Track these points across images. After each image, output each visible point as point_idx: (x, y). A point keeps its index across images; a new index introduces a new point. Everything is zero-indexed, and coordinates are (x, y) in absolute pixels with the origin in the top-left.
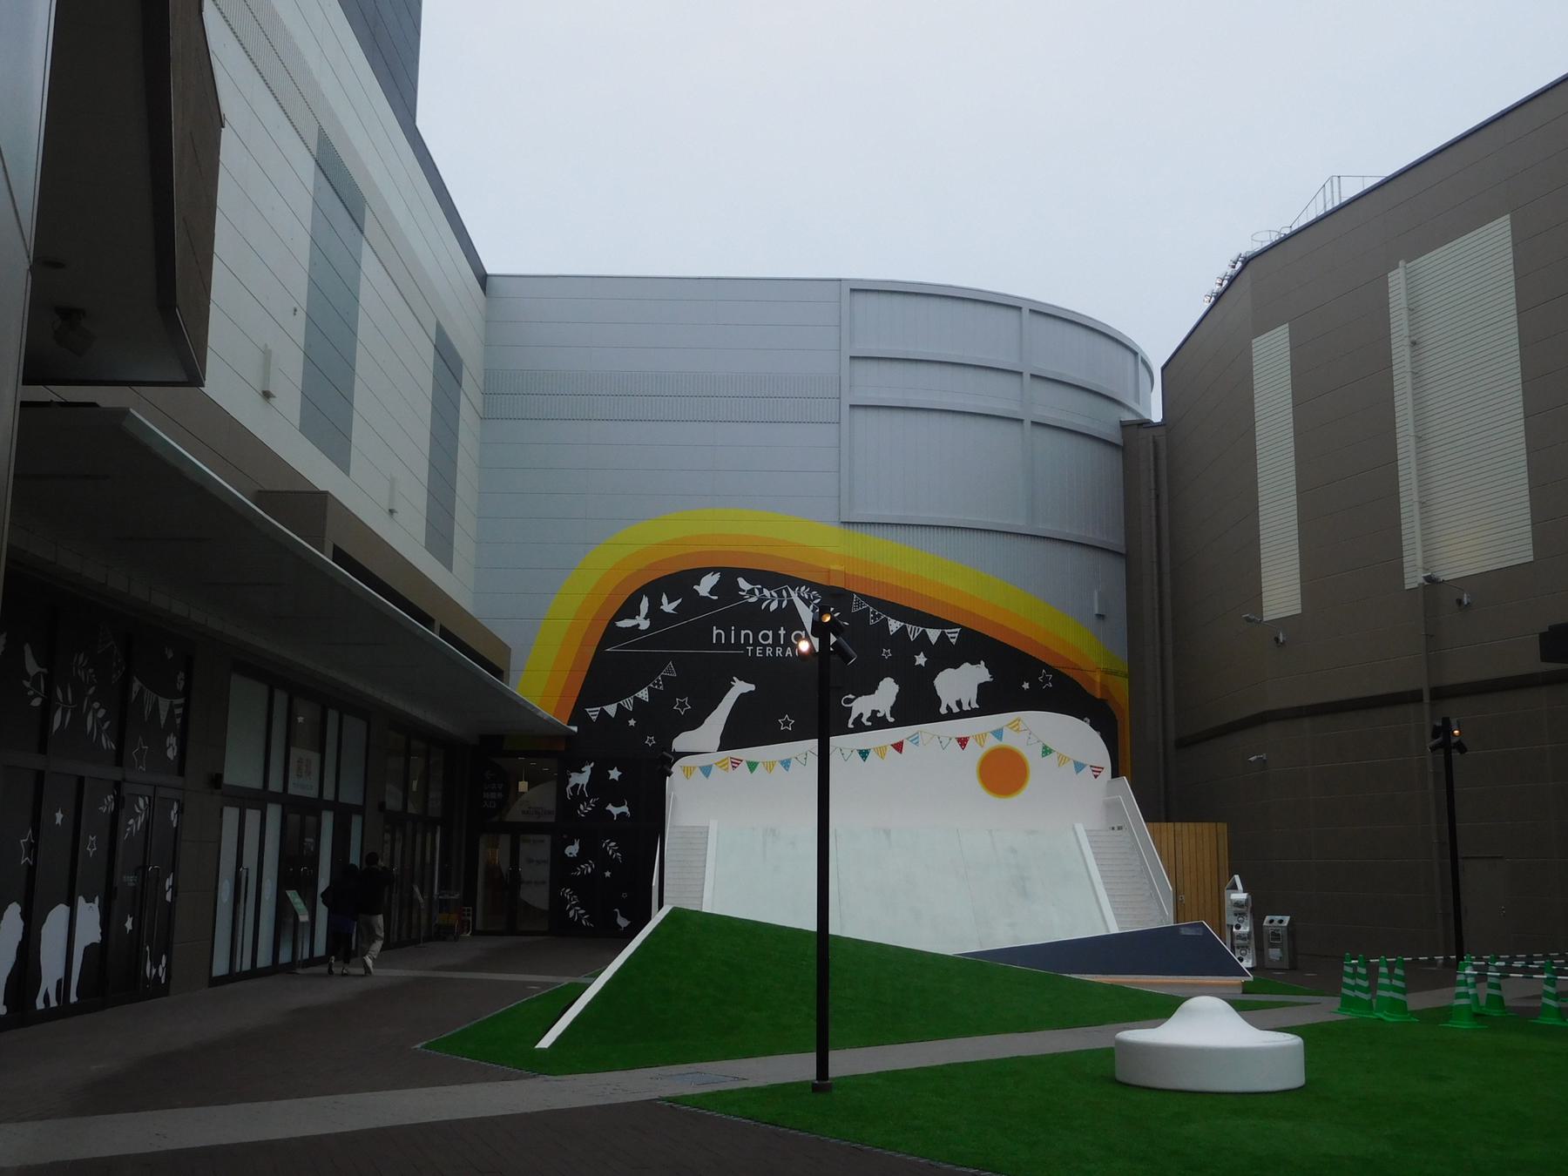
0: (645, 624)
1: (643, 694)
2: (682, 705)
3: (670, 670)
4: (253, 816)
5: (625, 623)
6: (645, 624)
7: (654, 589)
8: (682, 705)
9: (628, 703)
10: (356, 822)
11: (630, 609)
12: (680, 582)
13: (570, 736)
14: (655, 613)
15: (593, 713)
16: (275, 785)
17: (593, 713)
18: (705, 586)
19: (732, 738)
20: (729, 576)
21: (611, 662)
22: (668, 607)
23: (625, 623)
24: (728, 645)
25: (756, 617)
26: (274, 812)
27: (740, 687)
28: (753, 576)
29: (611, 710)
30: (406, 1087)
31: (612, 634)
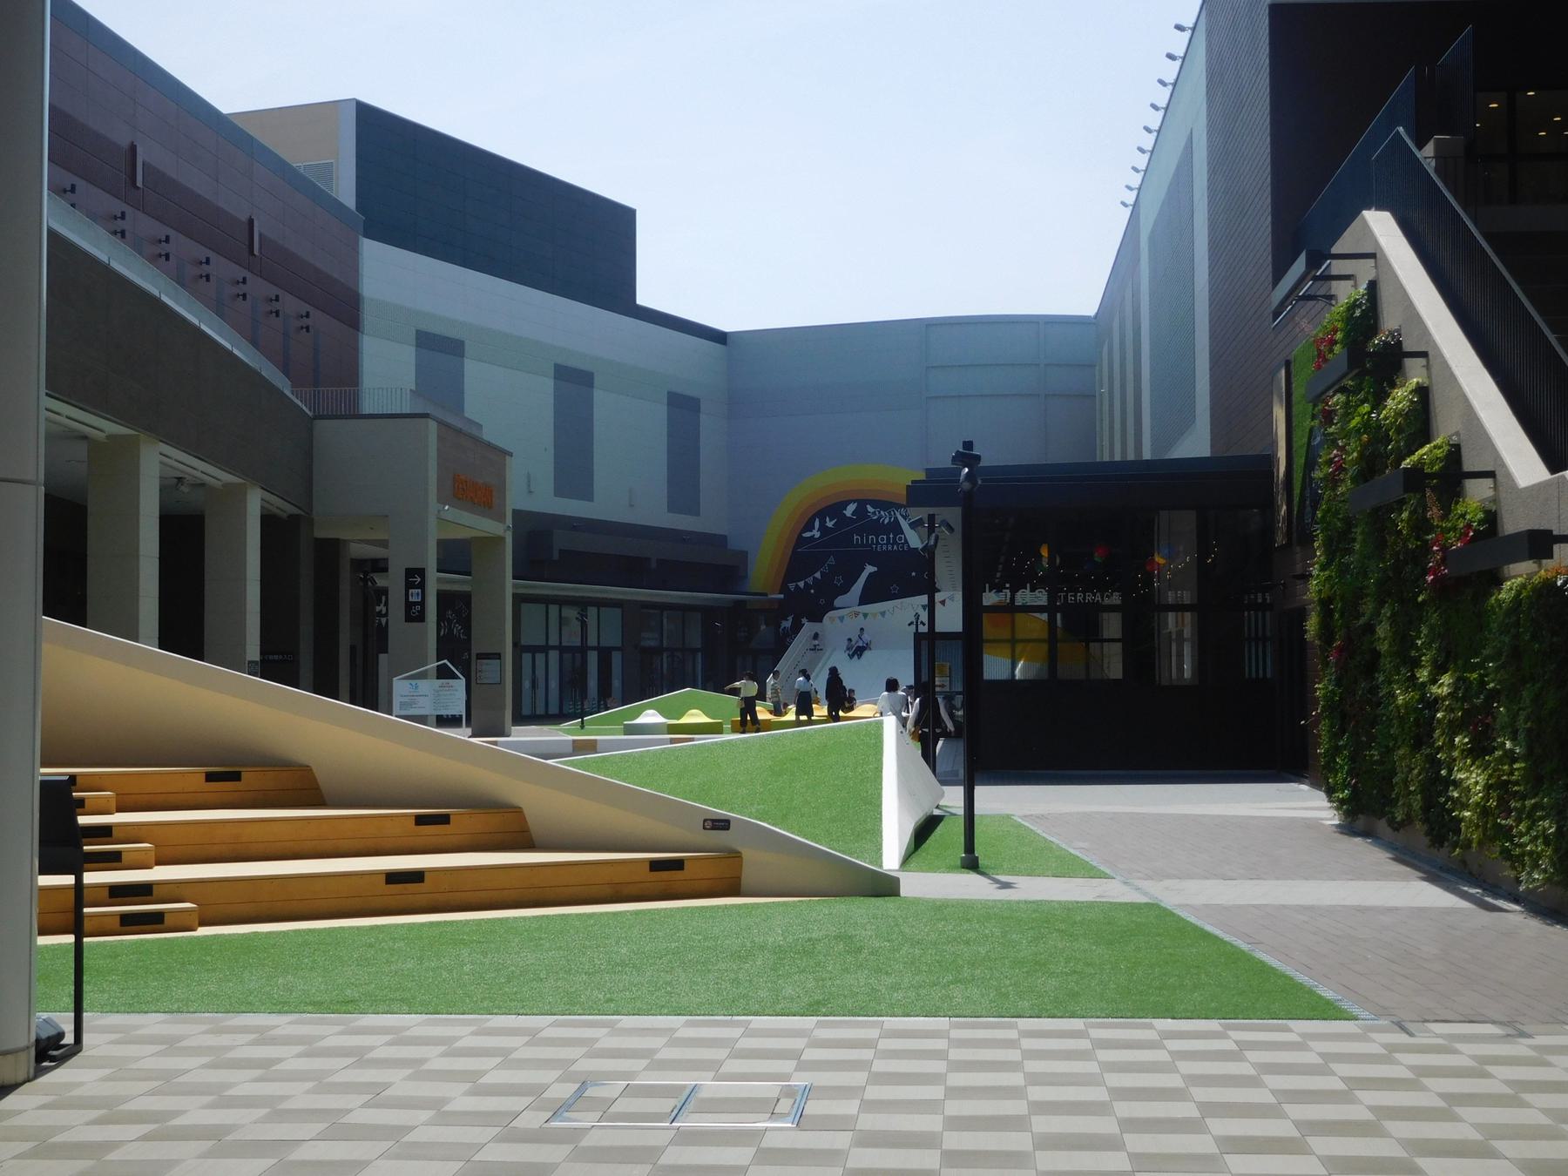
0: (817, 535)
1: (818, 575)
2: (839, 581)
3: (832, 560)
4: (540, 657)
5: (807, 534)
6: (817, 535)
7: (821, 514)
8: (839, 581)
9: (810, 580)
10: (616, 658)
11: (809, 526)
12: (835, 509)
13: (1439, 650)
14: (823, 528)
15: (792, 586)
16: (553, 641)
17: (792, 586)
18: (849, 511)
19: (865, 599)
20: (862, 504)
21: (801, 557)
22: (830, 524)
23: (807, 534)
24: (862, 545)
25: (877, 528)
26: (554, 656)
27: (870, 569)
28: (875, 504)
29: (801, 584)
30: (1272, 135)
31: (800, 541)
